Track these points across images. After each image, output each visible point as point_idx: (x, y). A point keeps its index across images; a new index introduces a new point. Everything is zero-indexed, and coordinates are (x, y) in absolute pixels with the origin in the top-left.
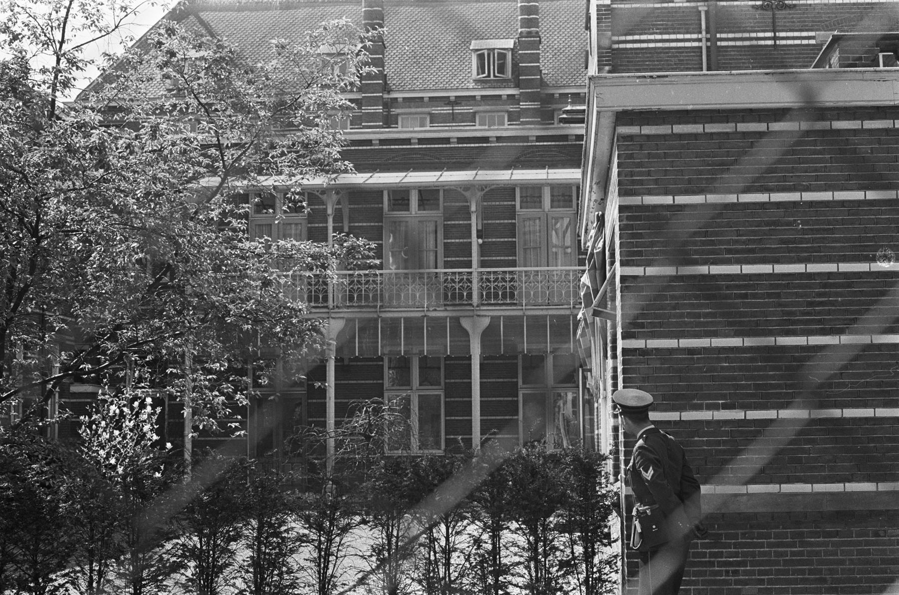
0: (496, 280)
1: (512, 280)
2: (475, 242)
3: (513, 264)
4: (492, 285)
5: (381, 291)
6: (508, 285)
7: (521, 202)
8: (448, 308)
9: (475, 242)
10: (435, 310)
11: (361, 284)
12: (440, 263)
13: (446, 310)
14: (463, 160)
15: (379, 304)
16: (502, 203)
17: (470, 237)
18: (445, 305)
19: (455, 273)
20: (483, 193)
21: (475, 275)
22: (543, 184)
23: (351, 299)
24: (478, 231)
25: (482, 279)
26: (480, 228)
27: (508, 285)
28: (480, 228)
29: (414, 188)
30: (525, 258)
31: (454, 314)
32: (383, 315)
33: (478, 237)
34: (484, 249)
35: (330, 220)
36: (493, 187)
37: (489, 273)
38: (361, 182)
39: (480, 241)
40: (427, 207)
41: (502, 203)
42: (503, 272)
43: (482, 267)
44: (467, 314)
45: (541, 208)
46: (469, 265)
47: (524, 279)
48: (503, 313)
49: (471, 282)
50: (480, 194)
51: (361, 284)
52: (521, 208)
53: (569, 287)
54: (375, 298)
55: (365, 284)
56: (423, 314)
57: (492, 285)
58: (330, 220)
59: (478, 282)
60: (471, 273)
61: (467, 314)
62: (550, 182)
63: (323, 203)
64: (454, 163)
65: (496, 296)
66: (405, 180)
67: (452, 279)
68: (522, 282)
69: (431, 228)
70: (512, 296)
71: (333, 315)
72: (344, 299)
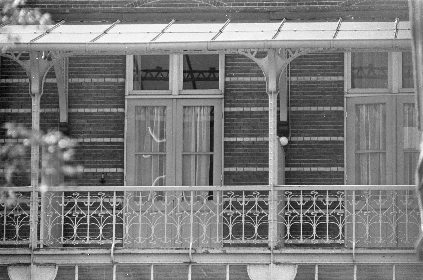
0: (308, 205)
1: (334, 205)
2: (274, 143)
3: (339, 178)
4: (301, 214)
5: (119, 220)
6: (327, 213)
7: (353, 77)
8: (228, 250)
9: (274, 143)
10: (207, 253)
11: (85, 209)
12: (218, 175)
13: (225, 253)
14: (257, 7)
15: (114, 243)
16: (321, 78)
17: (266, 133)
18: (225, 245)
19: (298, 192)
20: (289, 61)
21: (273, 195)
22: (387, 48)
23: (68, 232)
24: (280, 124)
25: (227, 203)
26: (284, 118)
27: (327, 213)
28: (284, 118)
29: (176, 51)
30: (358, 170)
31: (238, 260)
32: (121, 260)
33: (281, 133)
34: (289, 154)
35: (36, 103)
36: (303, 53)
37: (239, 193)
38: (88, 41)
39: (284, 140)
40: (198, 83)
41: (321, 78)
42: (236, 192)
43: (287, 182)
44: (13, 260)
45: (384, 86)
46: (263, 179)
47: (354, 203)
48: (156, 260)
49: (266, 208)
50: (282, 63)
51: (85, 209)
52: (353, 86)
53: (214, 219)
54: (107, 232)
55: (92, 209)
56: (186, 259)
57: (301, 214)
58: (36, 103)
59: (279, 208)
60: (266, 193)
61: (13, 260)
62: (399, 44)
63: (260, 74)
64: (244, 11)
65: (308, 231)
66: (162, 39)
67: (260, 203)
68: (350, 208)
69: (203, 117)
70: (334, 231)
71: (38, 260)
72: (55, 231)
